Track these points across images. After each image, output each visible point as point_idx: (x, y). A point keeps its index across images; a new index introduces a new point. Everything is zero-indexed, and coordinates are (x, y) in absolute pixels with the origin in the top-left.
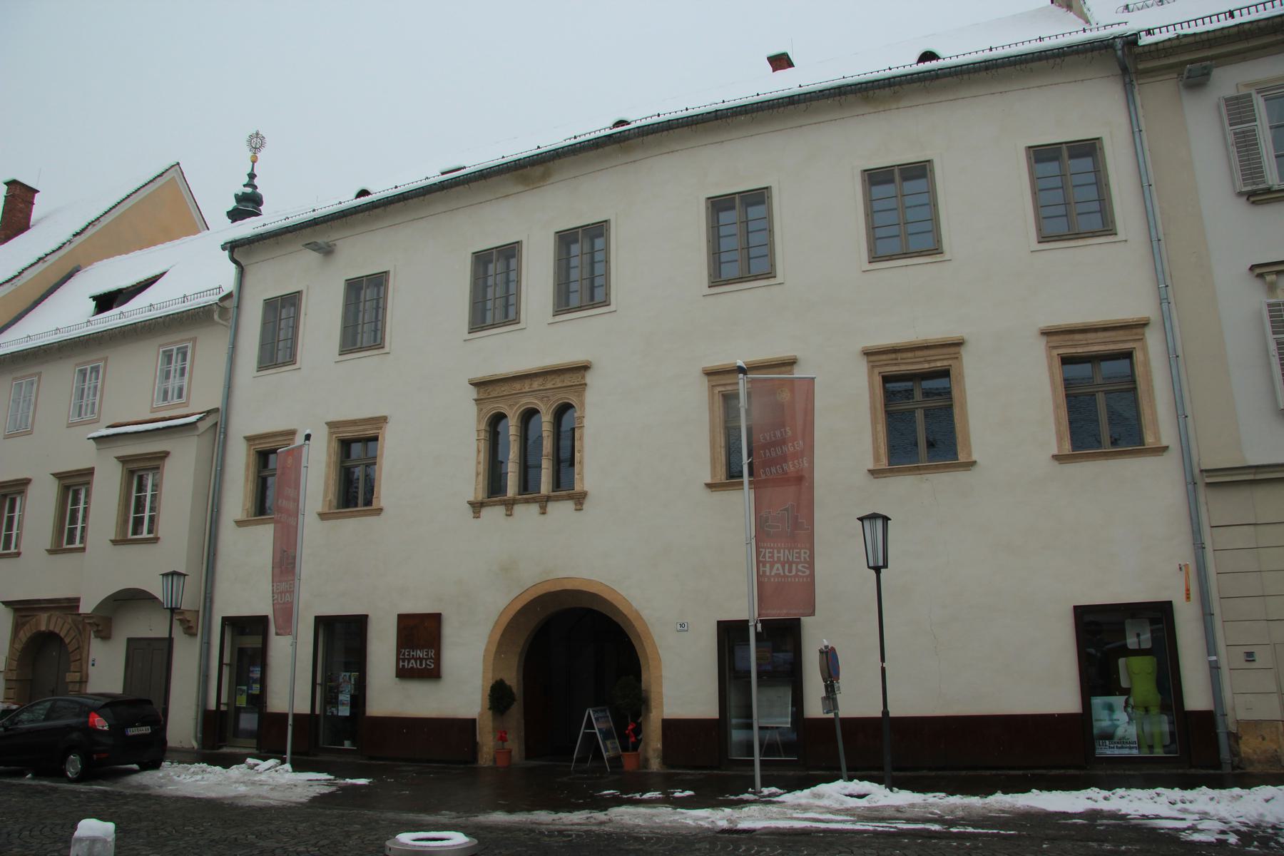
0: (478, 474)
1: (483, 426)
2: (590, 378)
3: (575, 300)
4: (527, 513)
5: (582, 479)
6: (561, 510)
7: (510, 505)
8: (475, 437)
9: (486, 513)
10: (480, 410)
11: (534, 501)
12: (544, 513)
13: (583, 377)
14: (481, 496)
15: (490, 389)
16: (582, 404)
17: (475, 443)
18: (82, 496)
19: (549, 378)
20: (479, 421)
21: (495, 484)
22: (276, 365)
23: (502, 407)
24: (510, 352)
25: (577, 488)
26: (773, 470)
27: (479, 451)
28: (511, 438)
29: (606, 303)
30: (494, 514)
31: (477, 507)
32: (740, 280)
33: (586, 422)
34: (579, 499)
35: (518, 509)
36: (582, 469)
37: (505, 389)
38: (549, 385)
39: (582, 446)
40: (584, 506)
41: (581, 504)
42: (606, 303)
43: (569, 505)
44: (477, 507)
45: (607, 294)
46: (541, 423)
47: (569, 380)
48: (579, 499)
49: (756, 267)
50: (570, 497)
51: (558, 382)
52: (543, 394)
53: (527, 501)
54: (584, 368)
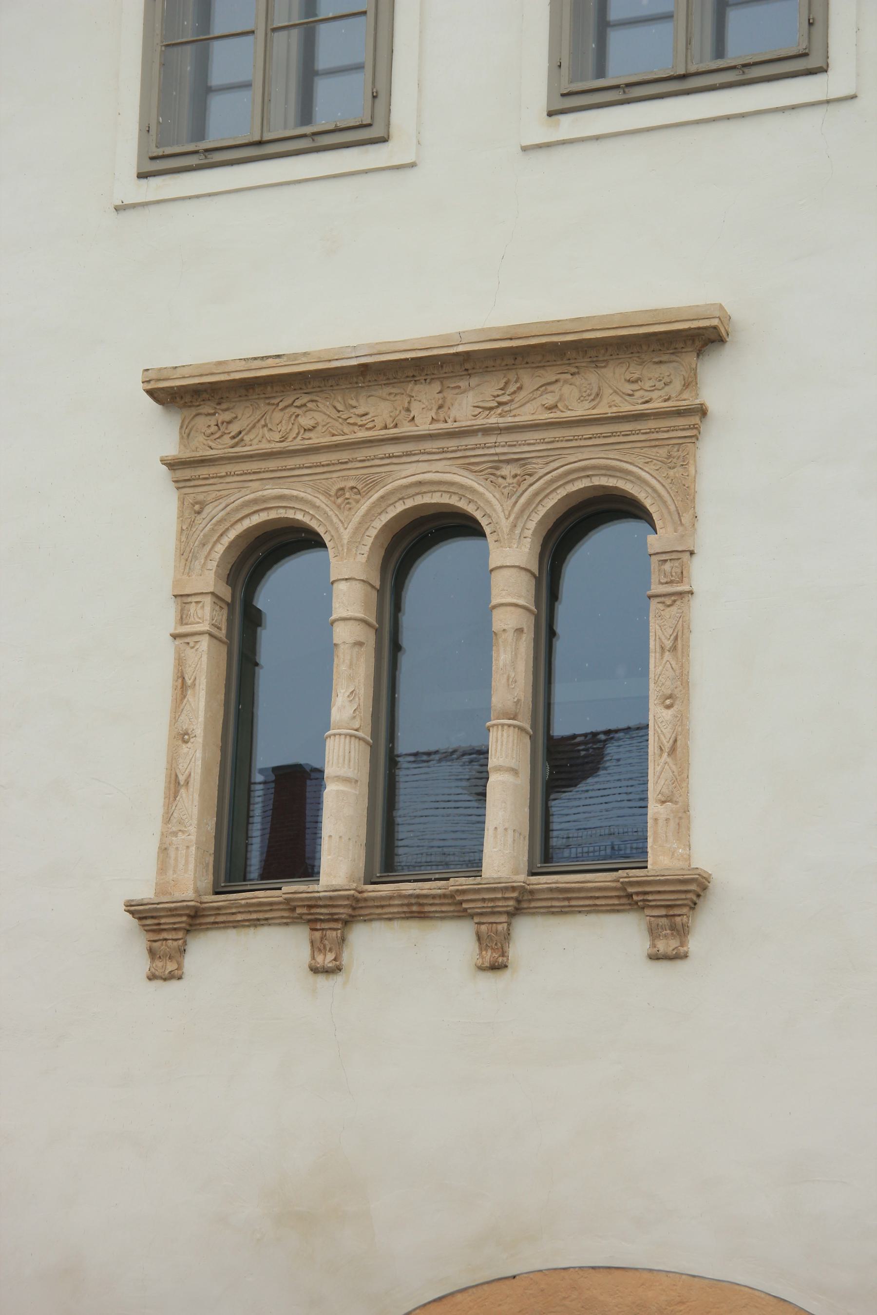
0: (175, 785)
1: (207, 577)
2: (719, 384)
3: (230, 118)
4: (413, 967)
5: (682, 820)
6: (581, 957)
7: (331, 923)
8: (167, 619)
9: (213, 957)
10: (193, 510)
11: (456, 908)
12: (497, 967)
13: (691, 383)
14: (190, 880)
15: (244, 416)
16: (686, 495)
17: (167, 650)
18: (446, 901)
19: (529, 380)
20: (186, 556)
21: (263, 831)
22: (211, 158)
23: (302, 500)
24: (315, 266)
25: (661, 860)
26: (260, 799)
27: (183, 686)
28: (343, 634)
29: (368, 131)
30: (252, 966)
31: (167, 929)
32: (680, 83)
33: (702, 575)
34: (672, 908)
35: (373, 946)
36: (681, 778)
37: (319, 420)
38: (527, 414)
39: (683, 678)
40: (694, 944)
41: (681, 932)
42: (368, 131)
43: (622, 937)
44: (167, 929)
45: (379, 95)
46: (485, 574)
47: (615, 390)
48: (672, 908)
49: (335, 102)
50: (630, 900)
51: (573, 395)
52: (501, 446)
53: (417, 911)
54: (701, 339)
